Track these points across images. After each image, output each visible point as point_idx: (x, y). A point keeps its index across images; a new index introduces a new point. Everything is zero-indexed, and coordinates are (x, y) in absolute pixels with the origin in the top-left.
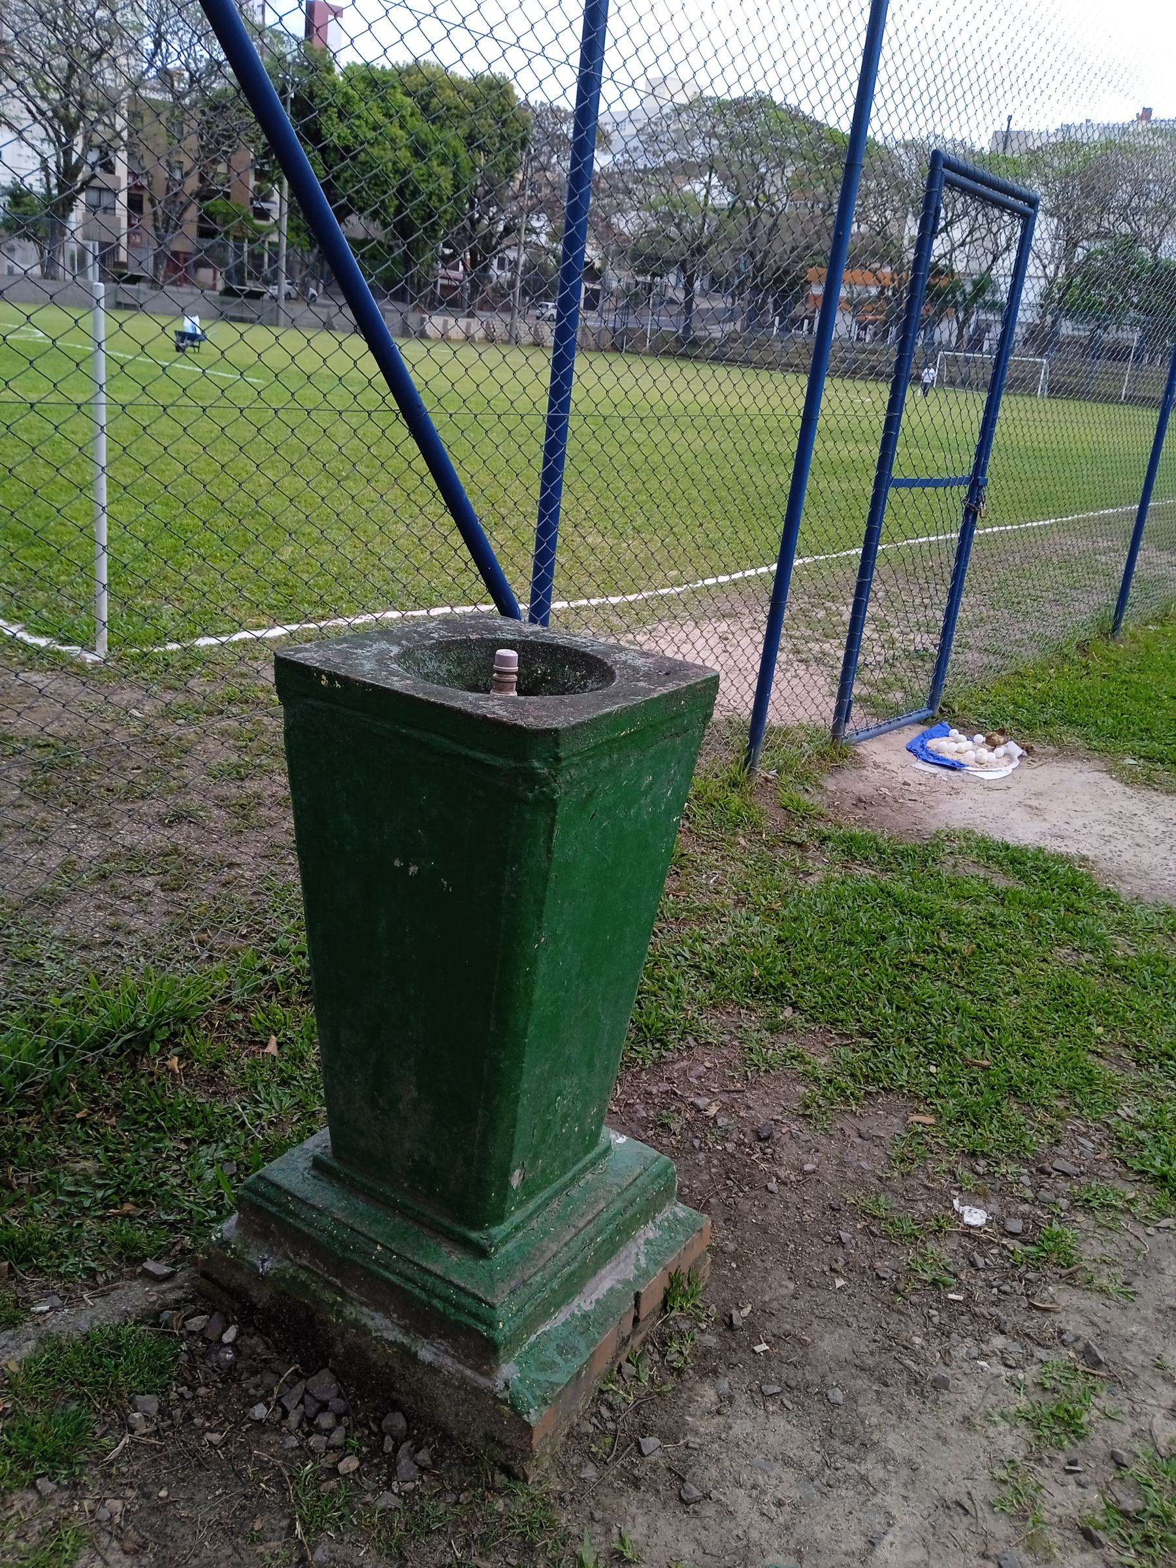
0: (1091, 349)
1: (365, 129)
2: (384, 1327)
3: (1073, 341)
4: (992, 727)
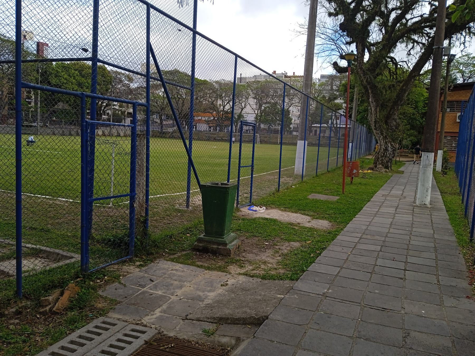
0: (269, 131)
1: (63, 80)
2: (215, 246)
3: (264, 129)
4: (261, 205)
